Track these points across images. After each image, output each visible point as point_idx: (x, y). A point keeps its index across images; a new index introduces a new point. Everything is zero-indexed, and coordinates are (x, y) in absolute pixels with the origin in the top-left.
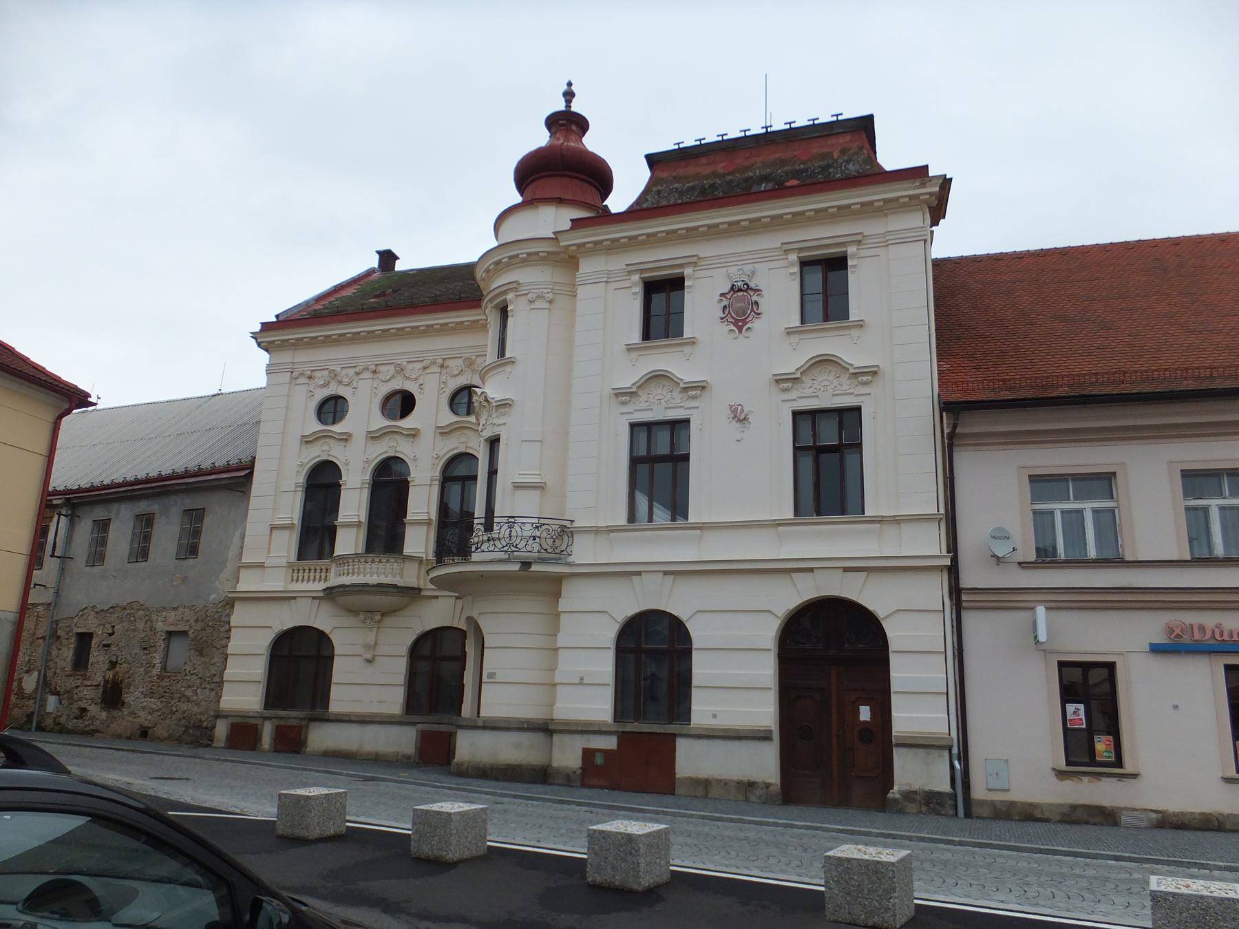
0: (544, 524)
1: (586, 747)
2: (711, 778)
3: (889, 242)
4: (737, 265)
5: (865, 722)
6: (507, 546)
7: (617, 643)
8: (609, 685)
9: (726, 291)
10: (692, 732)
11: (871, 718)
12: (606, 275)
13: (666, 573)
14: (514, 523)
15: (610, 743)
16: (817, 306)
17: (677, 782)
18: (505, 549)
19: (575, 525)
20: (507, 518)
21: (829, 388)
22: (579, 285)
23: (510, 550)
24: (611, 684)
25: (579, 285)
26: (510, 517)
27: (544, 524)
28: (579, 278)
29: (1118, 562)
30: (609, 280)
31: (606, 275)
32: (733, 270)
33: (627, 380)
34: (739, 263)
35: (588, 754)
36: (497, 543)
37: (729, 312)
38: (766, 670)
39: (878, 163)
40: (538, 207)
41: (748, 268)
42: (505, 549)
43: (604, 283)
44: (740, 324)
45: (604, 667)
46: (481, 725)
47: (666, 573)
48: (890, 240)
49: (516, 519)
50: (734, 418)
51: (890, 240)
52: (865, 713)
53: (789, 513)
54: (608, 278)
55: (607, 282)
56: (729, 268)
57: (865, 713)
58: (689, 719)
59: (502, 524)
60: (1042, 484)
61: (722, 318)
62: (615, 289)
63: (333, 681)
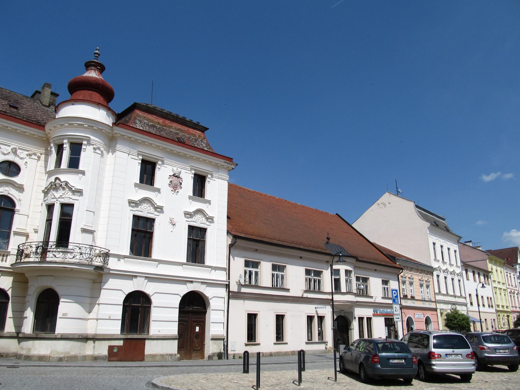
0: (103, 251)
1: (110, 345)
2: (157, 354)
3: (219, 178)
4: (176, 167)
5: (197, 332)
6: (88, 258)
7: (38, 299)
8: (153, 321)
9: (171, 175)
10: (150, 338)
11: (199, 331)
12: (129, 151)
13: (202, 283)
14: (92, 248)
15: (121, 343)
16: (197, 192)
17: (145, 357)
18: (87, 259)
19: (110, 252)
20: (89, 246)
21: (147, 210)
22: (117, 150)
23: (89, 260)
24: (152, 321)
25: (117, 150)
26: (91, 246)
27: (103, 251)
28: (118, 147)
29: (257, 287)
30: (130, 153)
31: (129, 151)
32: (175, 169)
33: (191, 210)
34: (177, 167)
35: (111, 348)
36: (84, 256)
37: (172, 183)
38: (175, 315)
39: (121, 113)
40: (100, 107)
41: (179, 170)
42: (87, 259)
43: (128, 154)
44: (175, 189)
45: (118, 312)
46: (60, 337)
47: (146, 277)
48: (219, 177)
49: (93, 247)
50: (171, 223)
51: (219, 177)
52: (197, 329)
53: (185, 261)
54: (130, 152)
55: (129, 154)
56: (174, 167)
57: (197, 329)
58: (55, 331)
59: (87, 248)
60: (308, 272)
61: (169, 184)
62: (131, 158)
63: (121, 321)
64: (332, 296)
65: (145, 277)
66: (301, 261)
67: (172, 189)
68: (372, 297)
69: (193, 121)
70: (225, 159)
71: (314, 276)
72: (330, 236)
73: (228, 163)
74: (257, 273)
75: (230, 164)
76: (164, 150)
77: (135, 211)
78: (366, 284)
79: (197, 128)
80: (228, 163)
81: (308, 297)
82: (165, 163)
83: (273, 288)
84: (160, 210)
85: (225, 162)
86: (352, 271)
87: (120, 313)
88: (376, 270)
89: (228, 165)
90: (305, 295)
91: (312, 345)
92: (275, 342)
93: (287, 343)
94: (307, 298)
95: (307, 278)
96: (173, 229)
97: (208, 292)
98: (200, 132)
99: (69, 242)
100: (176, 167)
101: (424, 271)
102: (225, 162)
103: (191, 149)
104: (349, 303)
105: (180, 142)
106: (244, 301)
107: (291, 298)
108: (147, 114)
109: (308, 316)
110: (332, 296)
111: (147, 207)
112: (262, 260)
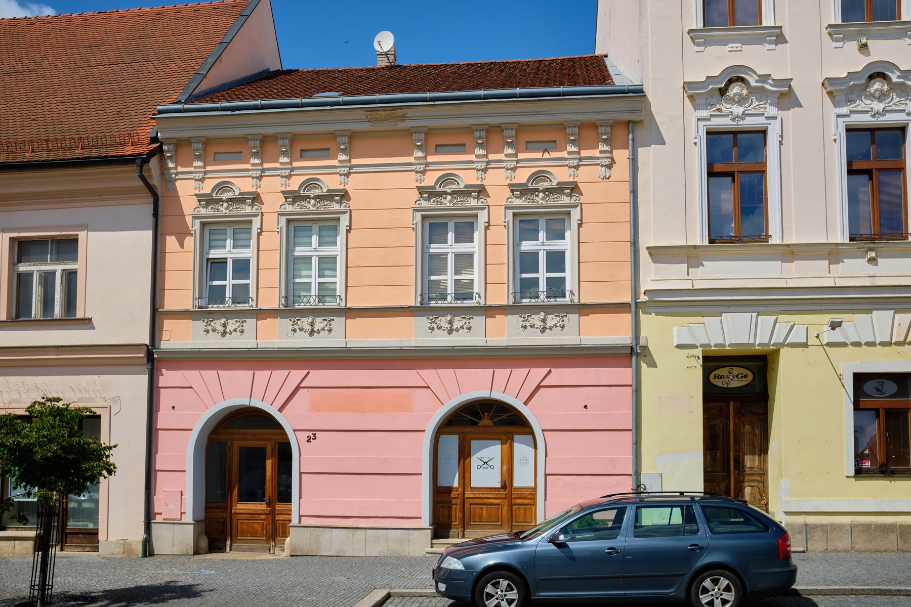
74: (71, 278)
101: (594, 126)
112: (85, 227)
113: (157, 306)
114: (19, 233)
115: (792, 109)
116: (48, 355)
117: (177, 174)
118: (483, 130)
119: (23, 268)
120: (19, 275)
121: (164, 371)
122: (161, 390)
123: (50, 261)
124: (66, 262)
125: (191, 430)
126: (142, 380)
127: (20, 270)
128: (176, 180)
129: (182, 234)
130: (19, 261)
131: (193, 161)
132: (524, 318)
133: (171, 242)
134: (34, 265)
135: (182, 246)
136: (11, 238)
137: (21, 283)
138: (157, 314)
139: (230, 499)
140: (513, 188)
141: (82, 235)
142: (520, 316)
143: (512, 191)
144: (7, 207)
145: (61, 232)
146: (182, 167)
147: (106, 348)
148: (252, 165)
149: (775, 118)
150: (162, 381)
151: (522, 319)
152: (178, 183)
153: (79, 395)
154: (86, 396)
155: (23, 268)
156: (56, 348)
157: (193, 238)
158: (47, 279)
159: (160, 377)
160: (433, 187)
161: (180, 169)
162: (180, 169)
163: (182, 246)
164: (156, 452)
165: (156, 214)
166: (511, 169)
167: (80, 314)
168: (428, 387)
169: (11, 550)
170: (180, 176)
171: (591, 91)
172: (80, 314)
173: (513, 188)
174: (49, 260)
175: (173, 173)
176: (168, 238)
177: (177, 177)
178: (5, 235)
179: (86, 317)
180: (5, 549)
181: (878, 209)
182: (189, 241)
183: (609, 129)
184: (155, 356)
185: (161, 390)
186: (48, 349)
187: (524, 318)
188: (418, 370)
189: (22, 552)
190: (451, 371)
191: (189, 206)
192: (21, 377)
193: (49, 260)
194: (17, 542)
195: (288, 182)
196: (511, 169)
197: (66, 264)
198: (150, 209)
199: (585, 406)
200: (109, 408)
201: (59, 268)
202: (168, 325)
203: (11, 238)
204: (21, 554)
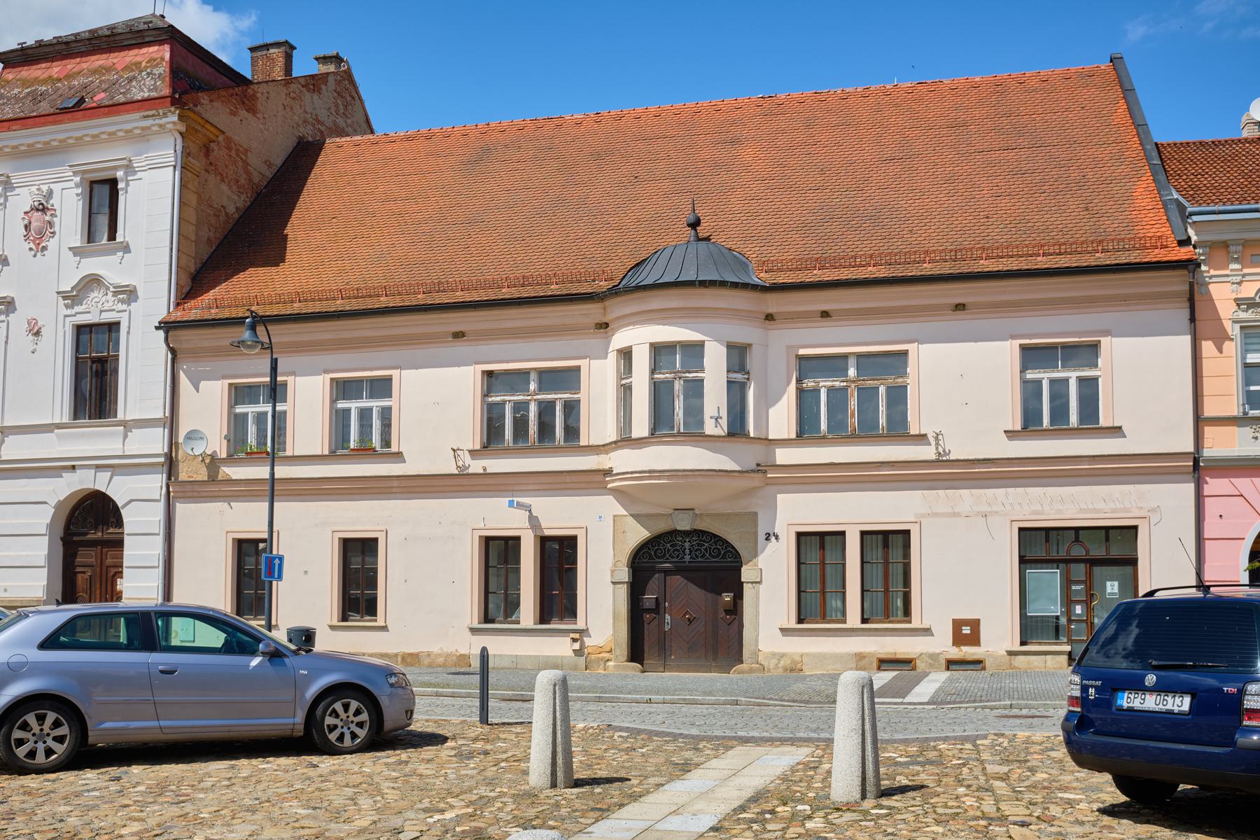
4: (35, 185)
34: (38, 183)
62: (141, 179)
64: (272, 469)
65: (94, 466)
66: (461, 348)
67: (32, 245)
68: (921, 438)
69: (25, 43)
70: (139, 110)
71: (541, 389)
72: (700, 213)
73: (153, 116)
74: (386, 414)
75: (159, 115)
76: (129, 136)
77: (75, 316)
78: (385, 403)
79: (147, 39)
80: (153, 116)
81: (489, 471)
82: (137, 169)
83: (332, 456)
84: (70, 301)
85: (145, 117)
86: (701, 345)
87: (40, 553)
88: (825, 314)
89: (157, 121)
90: (476, 466)
91: (65, 620)
92: (335, 622)
93: (384, 628)
94: (485, 475)
95: (552, 404)
96: (37, 344)
97: (119, 490)
98: (156, 48)
99: (1203, 356)
100: (35, 185)
101: (1225, 245)
102: (145, 117)
103: (44, 124)
104: (659, 478)
105: (77, 108)
106: (230, 504)
107: (395, 483)
108: (26, 68)
109: (488, 541)
110: (272, 469)
111: (96, 297)
112: (1107, 333)
113: (1199, 414)
114: (1030, 339)
115: (10, 315)
116: (1080, 465)
117: (1211, 277)
118: (1239, 245)
119: (240, 409)
120: (236, 415)
121: (1207, 479)
122: (1206, 498)
123: (1061, 368)
124: (1082, 368)
125: (1244, 539)
126: (1190, 488)
127: (1027, 377)
128: (1210, 283)
129: (1221, 338)
130: (236, 404)
131: (1230, 263)
132: (1255, 429)
133: (1208, 347)
134: (1045, 372)
135: (1220, 351)
136: (229, 384)
137: (1031, 392)
138: (1199, 421)
139: (1117, 612)
140: (1239, 302)
141: (1105, 342)
142: (1251, 428)
143: (1238, 305)
144: (1121, 308)
145: (1080, 338)
146: (1215, 269)
147: (1027, 461)
148: (1232, 270)
149: (126, 311)
150: (1207, 490)
151: (1254, 431)
152: (1211, 287)
153: (1112, 506)
154: (1119, 506)
155: (240, 409)
156: (1092, 458)
157: (1234, 343)
158: (365, 414)
159: (1205, 485)
160: (1253, 299)
161: (1213, 272)
162: (1213, 272)
163: (1220, 351)
164: (1204, 563)
165: (1193, 319)
166: (1237, 283)
167: (394, 449)
168: (1242, 495)
169: (1042, 664)
170: (1214, 280)
171: (1238, 210)
172: (394, 449)
173: (1239, 302)
174: (1060, 366)
175: (1207, 277)
176: (1204, 343)
177: (1211, 281)
178: (1014, 341)
179: (1116, 425)
180: (1036, 663)
181: (99, 386)
182: (1229, 347)
183: (1240, 248)
184: (1201, 464)
185: (1206, 498)
186: (1082, 459)
187: (1255, 429)
188: (1231, 479)
189: (1055, 666)
190: (1248, 480)
191: (1226, 310)
192: (1042, 488)
193: (1060, 366)
194: (1048, 657)
195: (1239, 288)
196: (1237, 283)
197: (1083, 370)
198: (1186, 313)
199: (1221, 516)
200: (919, 523)
201: (1073, 376)
202: (1209, 431)
203: (229, 384)
204: (1054, 668)
